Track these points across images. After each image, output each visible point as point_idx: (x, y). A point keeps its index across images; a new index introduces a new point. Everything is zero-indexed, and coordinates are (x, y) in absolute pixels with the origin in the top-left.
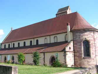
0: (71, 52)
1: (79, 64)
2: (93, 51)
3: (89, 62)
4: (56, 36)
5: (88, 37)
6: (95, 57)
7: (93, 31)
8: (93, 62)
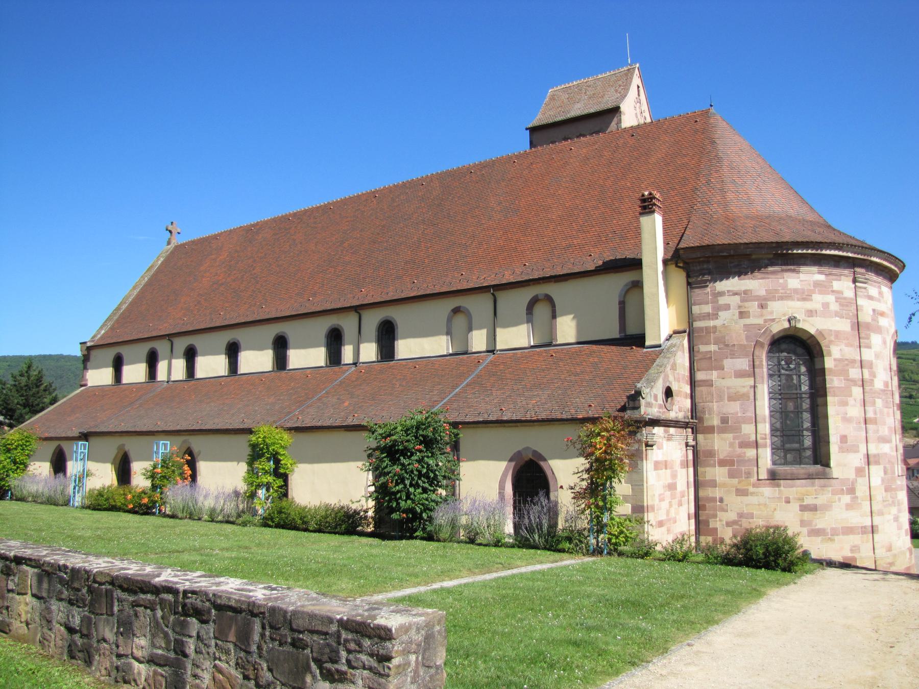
0: (676, 424)
1: (728, 524)
2: (846, 420)
3: (813, 508)
4: (549, 299)
5: (811, 313)
6: (859, 471)
7: (851, 263)
8: (849, 507)
